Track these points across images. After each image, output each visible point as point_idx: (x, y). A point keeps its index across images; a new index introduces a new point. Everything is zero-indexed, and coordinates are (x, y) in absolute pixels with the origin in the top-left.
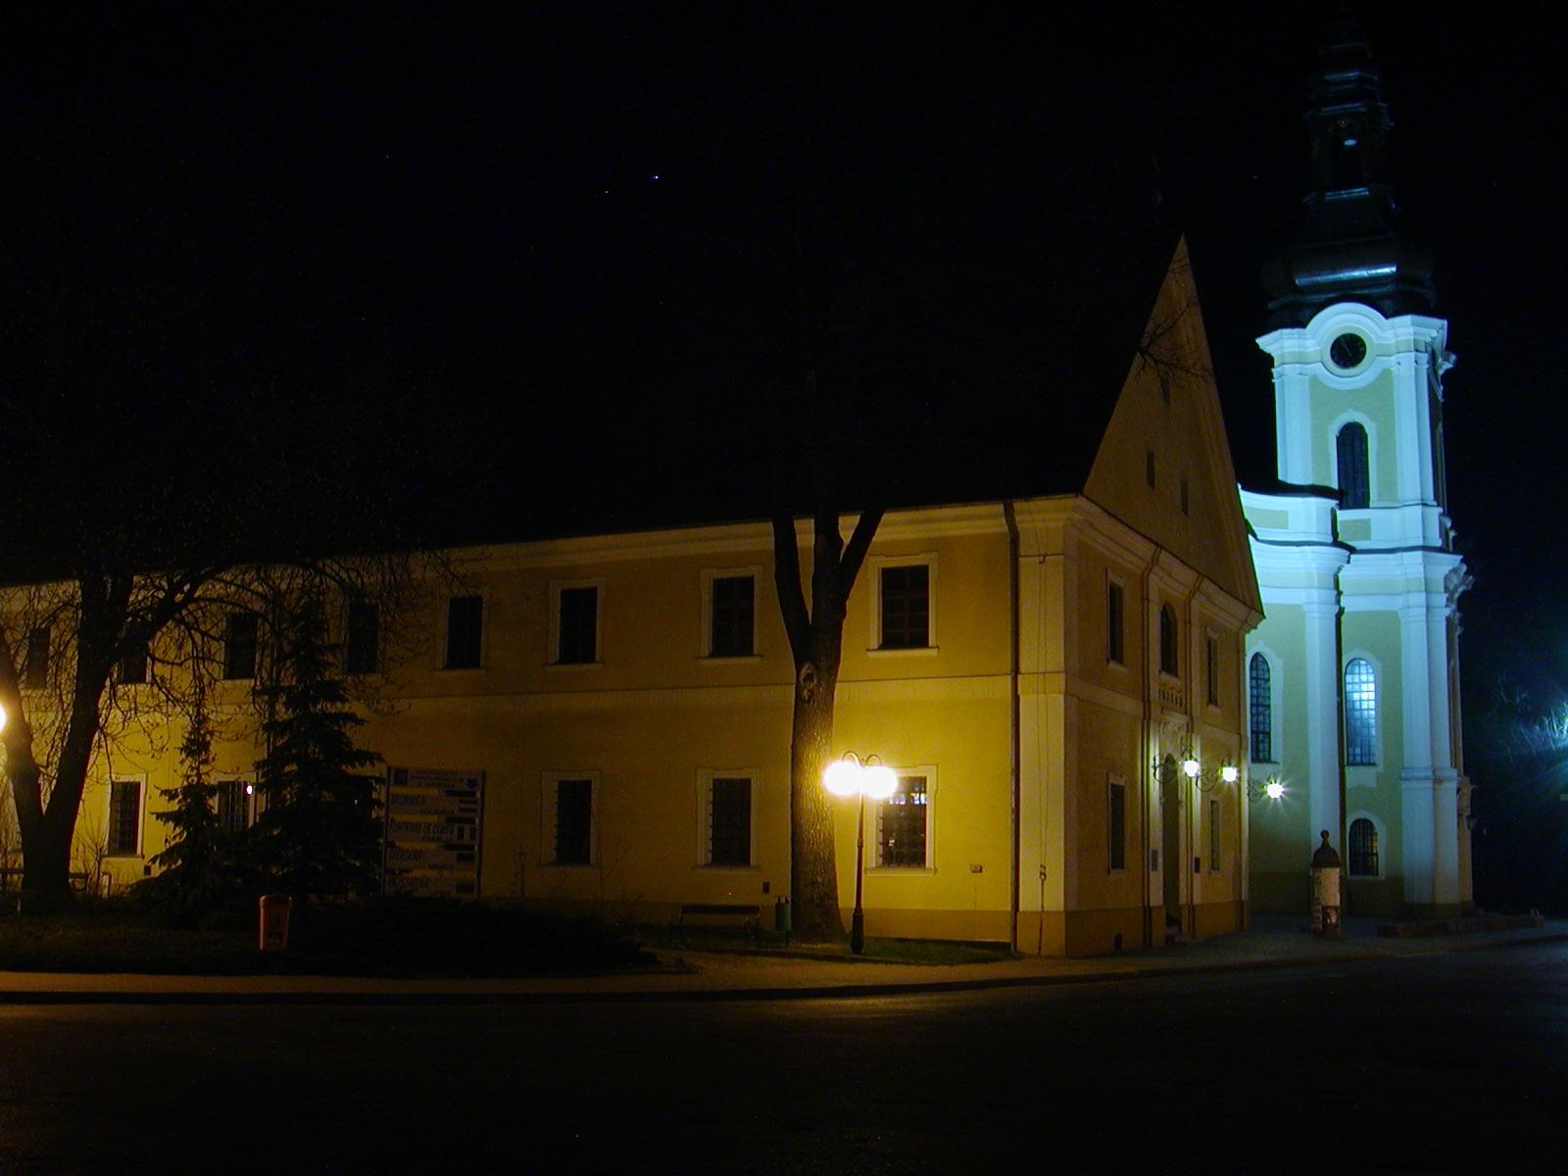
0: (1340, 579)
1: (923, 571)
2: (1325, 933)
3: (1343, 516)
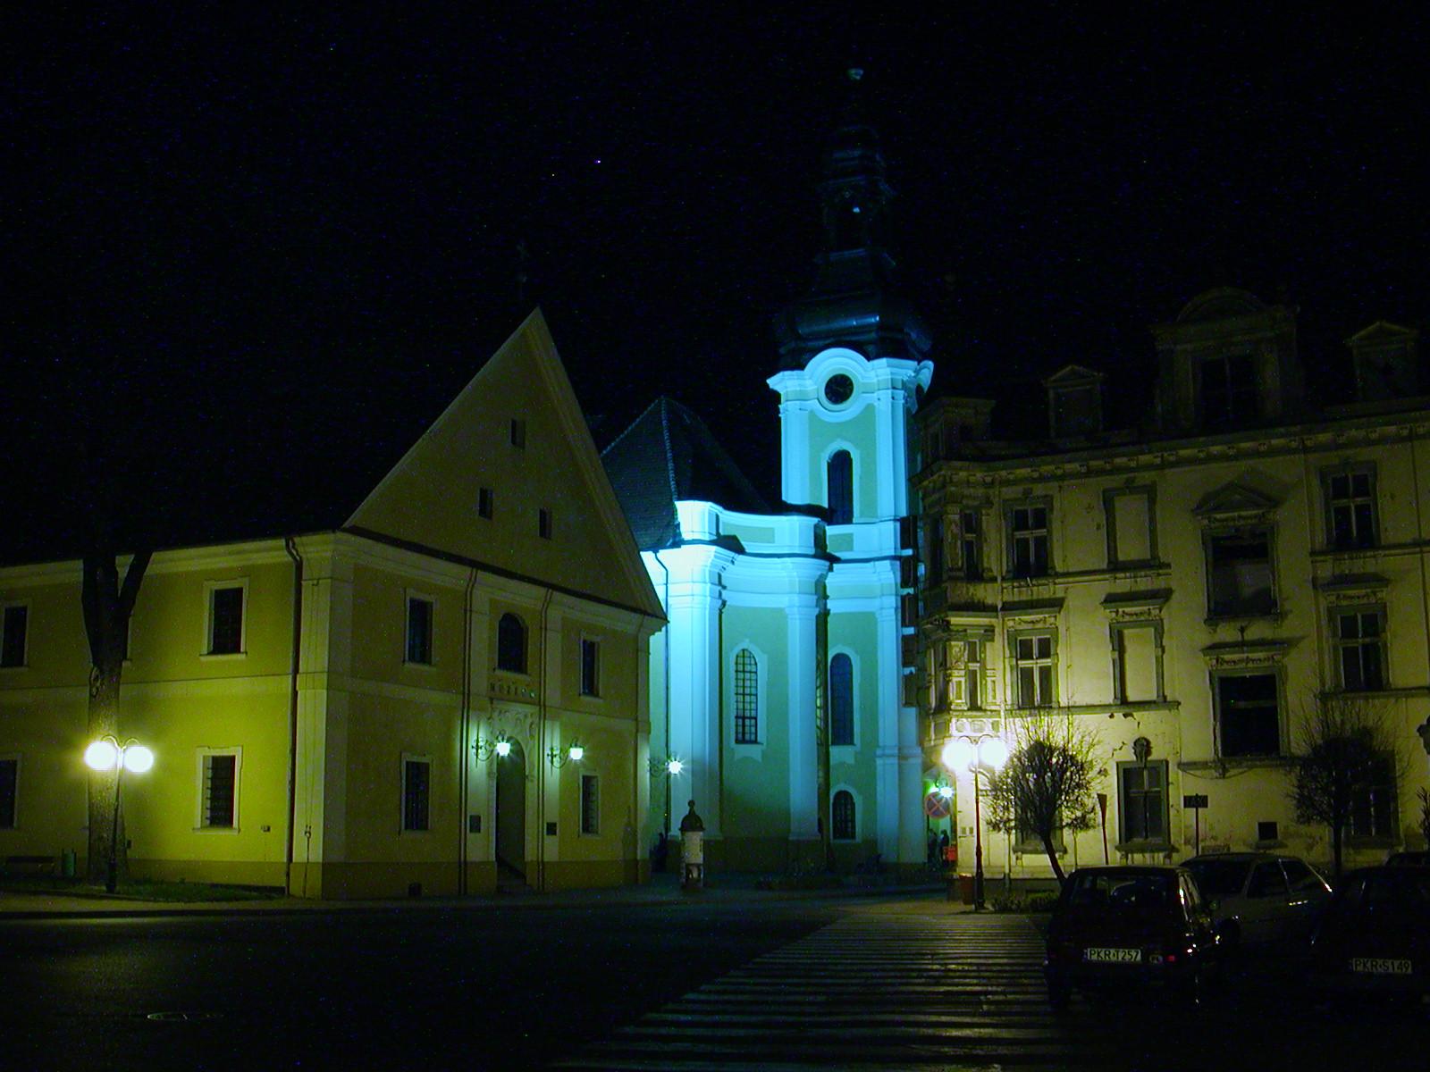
0: (827, 585)
1: (239, 591)
2: (688, 886)
3: (832, 531)
